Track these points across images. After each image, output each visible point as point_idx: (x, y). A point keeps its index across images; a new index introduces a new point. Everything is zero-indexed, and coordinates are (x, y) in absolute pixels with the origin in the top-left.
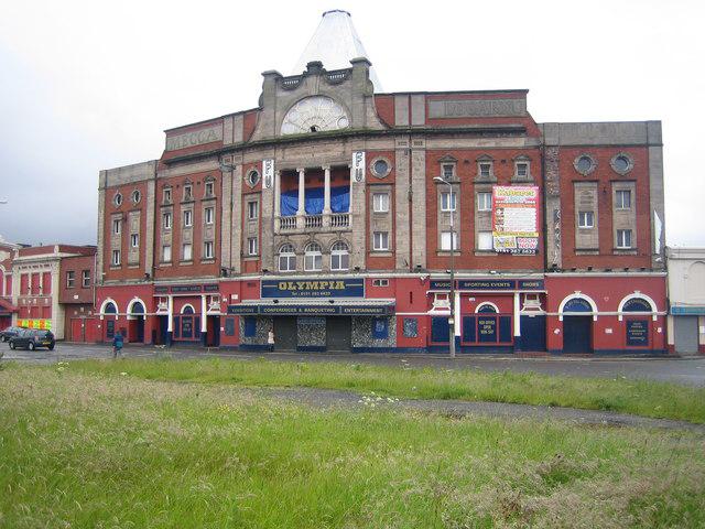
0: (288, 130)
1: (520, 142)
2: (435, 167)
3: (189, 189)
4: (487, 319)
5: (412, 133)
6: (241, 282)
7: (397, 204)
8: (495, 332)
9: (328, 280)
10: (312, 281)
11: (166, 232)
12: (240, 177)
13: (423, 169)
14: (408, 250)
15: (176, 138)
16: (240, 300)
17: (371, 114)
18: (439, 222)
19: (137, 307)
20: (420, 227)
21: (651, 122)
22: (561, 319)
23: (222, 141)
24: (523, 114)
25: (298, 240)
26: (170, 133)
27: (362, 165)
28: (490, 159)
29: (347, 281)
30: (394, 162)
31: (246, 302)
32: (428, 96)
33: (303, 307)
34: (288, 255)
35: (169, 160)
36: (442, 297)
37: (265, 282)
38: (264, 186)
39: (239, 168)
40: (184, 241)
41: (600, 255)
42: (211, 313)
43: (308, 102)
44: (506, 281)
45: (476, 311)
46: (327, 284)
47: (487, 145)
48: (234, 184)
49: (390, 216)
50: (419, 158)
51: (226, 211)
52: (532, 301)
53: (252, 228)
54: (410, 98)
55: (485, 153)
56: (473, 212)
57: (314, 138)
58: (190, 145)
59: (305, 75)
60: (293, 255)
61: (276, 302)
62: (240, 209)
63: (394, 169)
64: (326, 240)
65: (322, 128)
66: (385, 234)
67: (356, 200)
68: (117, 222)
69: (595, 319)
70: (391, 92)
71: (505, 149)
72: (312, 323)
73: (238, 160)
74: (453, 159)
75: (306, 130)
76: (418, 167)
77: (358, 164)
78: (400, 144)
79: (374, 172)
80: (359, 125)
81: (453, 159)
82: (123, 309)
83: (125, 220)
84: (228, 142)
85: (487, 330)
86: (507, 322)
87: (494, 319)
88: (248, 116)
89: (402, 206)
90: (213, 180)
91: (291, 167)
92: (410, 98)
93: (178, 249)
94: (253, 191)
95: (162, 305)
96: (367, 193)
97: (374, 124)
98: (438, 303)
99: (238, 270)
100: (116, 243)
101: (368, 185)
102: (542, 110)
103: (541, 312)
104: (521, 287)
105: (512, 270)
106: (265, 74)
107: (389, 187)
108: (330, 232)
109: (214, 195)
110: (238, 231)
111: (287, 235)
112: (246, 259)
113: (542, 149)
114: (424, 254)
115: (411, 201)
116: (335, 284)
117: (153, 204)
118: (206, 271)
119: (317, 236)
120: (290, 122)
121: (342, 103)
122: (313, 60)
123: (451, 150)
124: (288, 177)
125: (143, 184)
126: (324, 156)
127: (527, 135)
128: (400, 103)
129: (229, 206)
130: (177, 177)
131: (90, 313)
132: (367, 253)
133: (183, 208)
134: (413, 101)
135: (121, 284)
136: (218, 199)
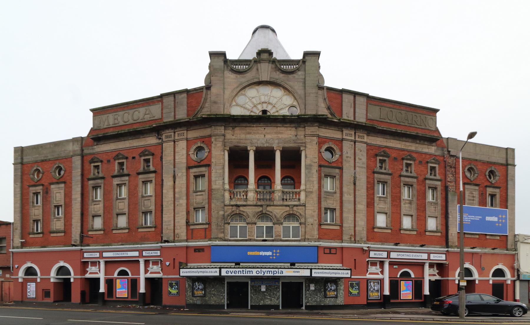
0: (236, 111)
1: (432, 150)
2: (373, 159)
3: (121, 164)
5: (356, 127)
6: (187, 247)
11: (96, 202)
13: (364, 159)
15: (104, 117)
18: (376, 205)
19: (62, 270)
20: (362, 207)
24: (434, 129)
25: (249, 211)
26: (97, 112)
28: (412, 159)
30: (341, 150)
35: (97, 137)
40: (118, 211)
41: (478, 239)
42: (149, 275)
45: (398, 276)
47: (410, 148)
49: (338, 195)
50: (361, 148)
51: (168, 183)
52: (374, 267)
53: (199, 199)
55: (410, 156)
56: (400, 199)
57: (264, 119)
58: (122, 123)
59: (256, 61)
62: (184, 181)
63: (341, 156)
64: (278, 212)
65: (272, 112)
68: (37, 194)
69: (477, 282)
70: (340, 87)
71: (421, 153)
75: (257, 112)
77: (309, 157)
78: (348, 134)
79: (194, 157)
80: (311, 112)
82: (46, 271)
83: (47, 192)
88: (190, 94)
89: (348, 188)
92: (355, 97)
95: (91, 269)
96: (319, 172)
99: (184, 236)
100: (36, 212)
101: (320, 166)
102: (449, 127)
103: (438, 277)
106: (212, 55)
107: (337, 171)
110: (183, 202)
111: (238, 206)
112: (192, 227)
114: (365, 229)
115: (355, 184)
117: (79, 178)
119: (269, 209)
124: (237, 158)
125: (68, 159)
126: (276, 138)
127: (437, 146)
128: (347, 99)
129: (171, 179)
130: (106, 153)
131: (8, 276)
132: (320, 225)
133: (116, 181)
135: (41, 221)
136: (158, 173)
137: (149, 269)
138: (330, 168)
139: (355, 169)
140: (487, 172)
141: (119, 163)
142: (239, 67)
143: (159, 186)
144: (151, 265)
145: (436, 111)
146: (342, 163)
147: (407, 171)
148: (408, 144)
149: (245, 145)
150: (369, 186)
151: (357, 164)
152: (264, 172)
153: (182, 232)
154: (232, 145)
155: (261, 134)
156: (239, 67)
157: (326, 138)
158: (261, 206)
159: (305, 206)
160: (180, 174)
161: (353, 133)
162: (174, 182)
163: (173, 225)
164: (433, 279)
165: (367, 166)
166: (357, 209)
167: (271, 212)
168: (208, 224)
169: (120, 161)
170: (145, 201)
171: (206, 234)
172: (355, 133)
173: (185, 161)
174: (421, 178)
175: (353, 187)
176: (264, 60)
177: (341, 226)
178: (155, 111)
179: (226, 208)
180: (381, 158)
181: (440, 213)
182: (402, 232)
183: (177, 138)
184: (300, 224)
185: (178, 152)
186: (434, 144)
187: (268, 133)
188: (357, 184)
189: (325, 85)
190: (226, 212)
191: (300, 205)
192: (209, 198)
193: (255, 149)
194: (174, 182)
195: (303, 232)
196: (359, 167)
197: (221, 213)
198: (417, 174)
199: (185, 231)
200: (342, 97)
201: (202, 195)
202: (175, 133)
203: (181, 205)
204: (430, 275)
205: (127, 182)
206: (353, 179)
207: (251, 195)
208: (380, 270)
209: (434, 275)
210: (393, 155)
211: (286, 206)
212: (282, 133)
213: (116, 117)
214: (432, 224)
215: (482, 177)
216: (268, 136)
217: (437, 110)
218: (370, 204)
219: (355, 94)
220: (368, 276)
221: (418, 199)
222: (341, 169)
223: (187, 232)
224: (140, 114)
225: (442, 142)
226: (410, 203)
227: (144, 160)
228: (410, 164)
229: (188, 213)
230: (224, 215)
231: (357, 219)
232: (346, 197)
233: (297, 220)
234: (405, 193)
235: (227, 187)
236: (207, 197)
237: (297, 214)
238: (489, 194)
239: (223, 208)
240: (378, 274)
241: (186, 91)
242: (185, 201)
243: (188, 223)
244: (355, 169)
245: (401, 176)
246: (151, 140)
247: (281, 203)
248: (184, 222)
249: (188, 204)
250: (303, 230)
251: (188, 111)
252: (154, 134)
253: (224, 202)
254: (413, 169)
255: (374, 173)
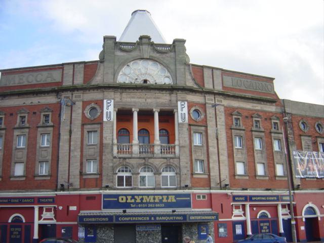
1: (272, 108)
2: (230, 118)
4: (264, 222)
6: (80, 196)
7: (209, 141)
8: (21, 237)
9: (162, 195)
10: (148, 195)
12: (80, 111)
14: (218, 174)
15: (11, 76)
16: (79, 209)
17: (189, 77)
18: (235, 155)
20: (224, 158)
21: (289, 101)
22: (304, 220)
23: (62, 82)
27: (185, 110)
29: (177, 196)
30: (205, 111)
31: (83, 213)
32: (224, 72)
33: (155, 216)
34: (125, 174)
36: (237, 207)
37: (106, 196)
38: (105, 119)
39: (79, 104)
41: (316, 181)
42: (42, 222)
43: (141, 62)
44: (274, 196)
45: (10, 221)
46: (161, 198)
47: (257, 108)
48: (73, 116)
49: (205, 148)
50: (220, 109)
51: (64, 136)
52: (237, 210)
54: (74, 66)
57: (145, 87)
58: (26, 83)
60: (128, 174)
61: (125, 212)
63: (206, 116)
65: (151, 81)
66: (202, 161)
67: (181, 136)
69: (319, 219)
72: (149, 229)
73: (80, 98)
74: (239, 114)
75: (140, 82)
76: (221, 117)
77: (182, 112)
78: (210, 99)
79: (88, 115)
81: (239, 114)
84: (67, 83)
85: (265, 229)
86: (275, 223)
87: (268, 221)
89: (212, 142)
90: (57, 110)
91: (127, 107)
93: (10, 166)
94: (94, 121)
96: (190, 130)
97: (190, 84)
98: (236, 212)
101: (190, 125)
102: (283, 91)
103: (54, 222)
104: (251, 200)
105: (281, 189)
106: (105, 38)
108: (140, 158)
109: (51, 123)
111: (125, 158)
113: (284, 113)
114: (228, 177)
115: (217, 139)
116: (167, 199)
118: (40, 186)
119: (151, 161)
120: (125, 74)
121: (166, 66)
122: (142, 35)
123: (237, 108)
124: (124, 115)
126: (156, 102)
127: (276, 105)
132: (192, 174)
133: (16, 133)
134: (75, 67)
137: (42, 215)
138: (198, 124)
139: (217, 127)
140: (316, 125)
141: (21, 117)
142: (125, 47)
143: (57, 137)
144: (44, 212)
145: (272, 79)
146: (206, 121)
147: (257, 126)
148: (255, 105)
149: (131, 107)
150: (229, 140)
151: (218, 123)
152: (146, 125)
153: (76, 182)
154: (119, 108)
155: (143, 98)
156: (125, 47)
157: (193, 102)
158: (144, 158)
159: (179, 158)
160: (75, 130)
161: (213, 98)
162: (70, 136)
163: (67, 175)
164: (286, 218)
165: (226, 124)
166: (220, 159)
167: (152, 164)
168: (100, 174)
169: (23, 115)
170: (43, 152)
171: (97, 182)
172: (215, 98)
173: (80, 118)
174: (268, 131)
175: (216, 141)
176: (145, 44)
177: (209, 175)
178: (56, 76)
179: (115, 160)
180: (236, 117)
181: (285, 161)
182: (277, 178)
183: (74, 99)
184: (176, 174)
185: (74, 111)
186: (274, 104)
187: (149, 98)
188: (219, 139)
189: (190, 63)
190: (115, 163)
191: (175, 158)
192: (100, 152)
193: (138, 110)
194: (70, 136)
195: (179, 181)
196: (220, 125)
197: (111, 165)
198: (265, 129)
199: (79, 180)
200: (203, 71)
201: (94, 148)
202: (72, 94)
203: (75, 156)
204: (283, 215)
205: (27, 134)
206: (215, 134)
207: (136, 149)
208: (243, 212)
209: (287, 215)
210: (245, 114)
211: (164, 158)
212: (159, 98)
213: (21, 77)
214: (280, 170)
215: (312, 130)
216: (149, 101)
217: (274, 79)
218: (231, 155)
219: (213, 69)
220: (234, 219)
221: (267, 150)
222: (206, 127)
223: (80, 182)
224: (42, 78)
225: (280, 102)
226: (262, 152)
227: (44, 115)
228: (258, 121)
229: (81, 164)
230: (112, 167)
231: (221, 168)
232: (211, 149)
233: (174, 171)
234: (257, 145)
235: (115, 141)
236: (98, 150)
237: (174, 165)
238: (320, 143)
239: (112, 160)
240: (241, 216)
241: (84, 63)
242: (80, 153)
243: (81, 174)
244: (217, 127)
245: (252, 131)
246: (51, 99)
247: (160, 155)
248: (78, 172)
249: (82, 156)
250: (179, 179)
251: (84, 77)
252: (54, 93)
253: (113, 155)
254: (261, 125)
255: (231, 129)
